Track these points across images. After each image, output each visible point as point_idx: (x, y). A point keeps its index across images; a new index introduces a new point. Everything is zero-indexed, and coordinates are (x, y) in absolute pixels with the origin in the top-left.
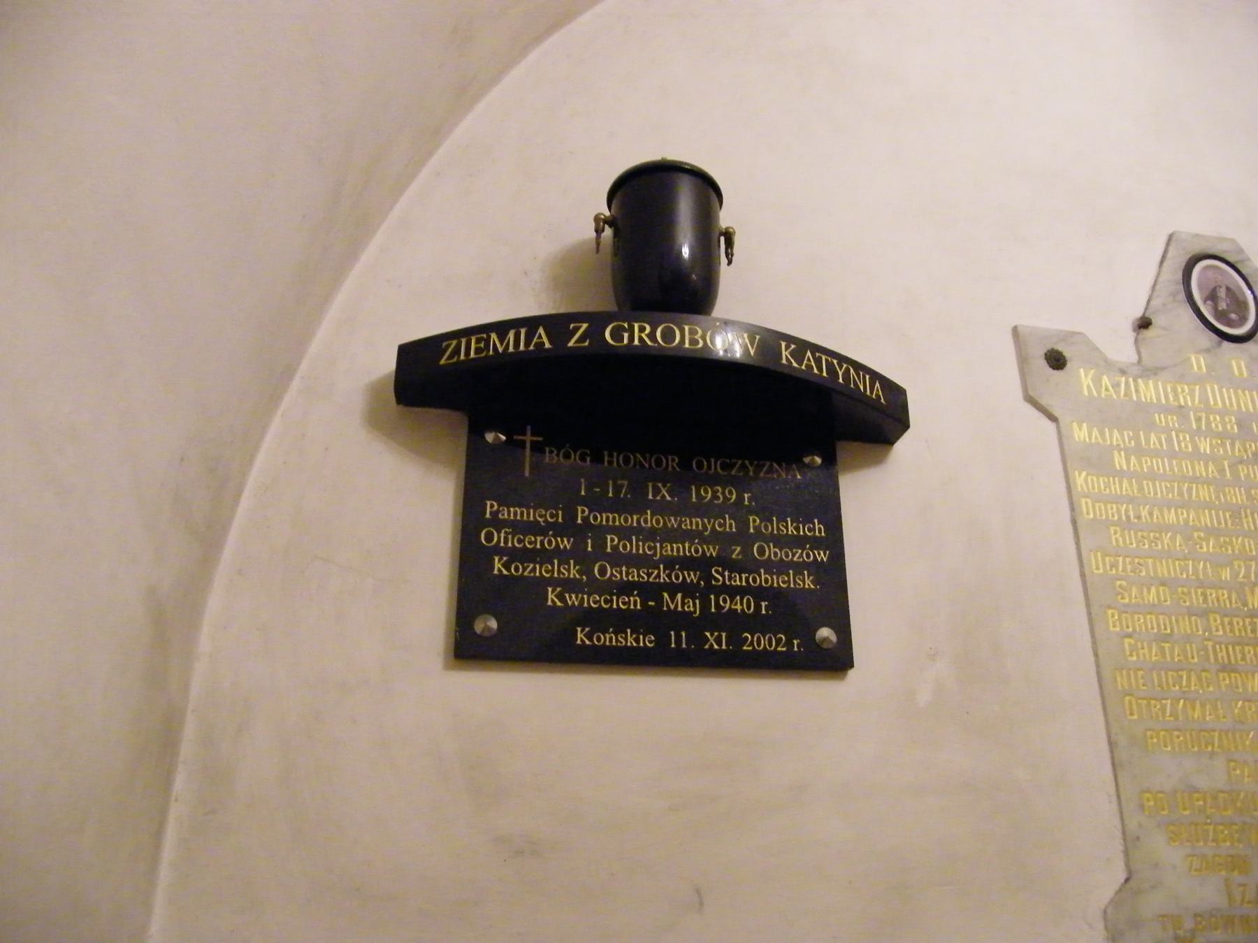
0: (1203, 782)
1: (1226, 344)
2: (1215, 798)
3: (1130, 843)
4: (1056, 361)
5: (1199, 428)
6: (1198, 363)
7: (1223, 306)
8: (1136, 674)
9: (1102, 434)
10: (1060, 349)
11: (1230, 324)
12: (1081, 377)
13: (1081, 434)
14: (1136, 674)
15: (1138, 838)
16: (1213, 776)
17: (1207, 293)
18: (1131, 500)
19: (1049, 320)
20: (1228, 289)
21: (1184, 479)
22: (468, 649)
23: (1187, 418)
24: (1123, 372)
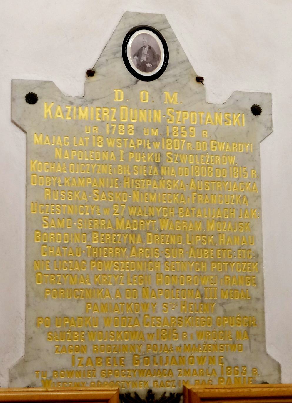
0: (71, 313)
1: (140, 82)
2: (75, 320)
3: (29, 339)
4: (32, 99)
5: (110, 133)
6: (119, 95)
7: (144, 58)
8: (102, 249)
9: (51, 139)
10: (33, 92)
11: (145, 70)
12: (45, 107)
13: (37, 139)
14: (102, 249)
15: (32, 338)
16: (76, 309)
17: (136, 51)
18: (60, 175)
19: (32, 75)
20: (150, 48)
21: (95, 162)
22: (12, 82)
23: (104, 128)
24: (71, 103)
